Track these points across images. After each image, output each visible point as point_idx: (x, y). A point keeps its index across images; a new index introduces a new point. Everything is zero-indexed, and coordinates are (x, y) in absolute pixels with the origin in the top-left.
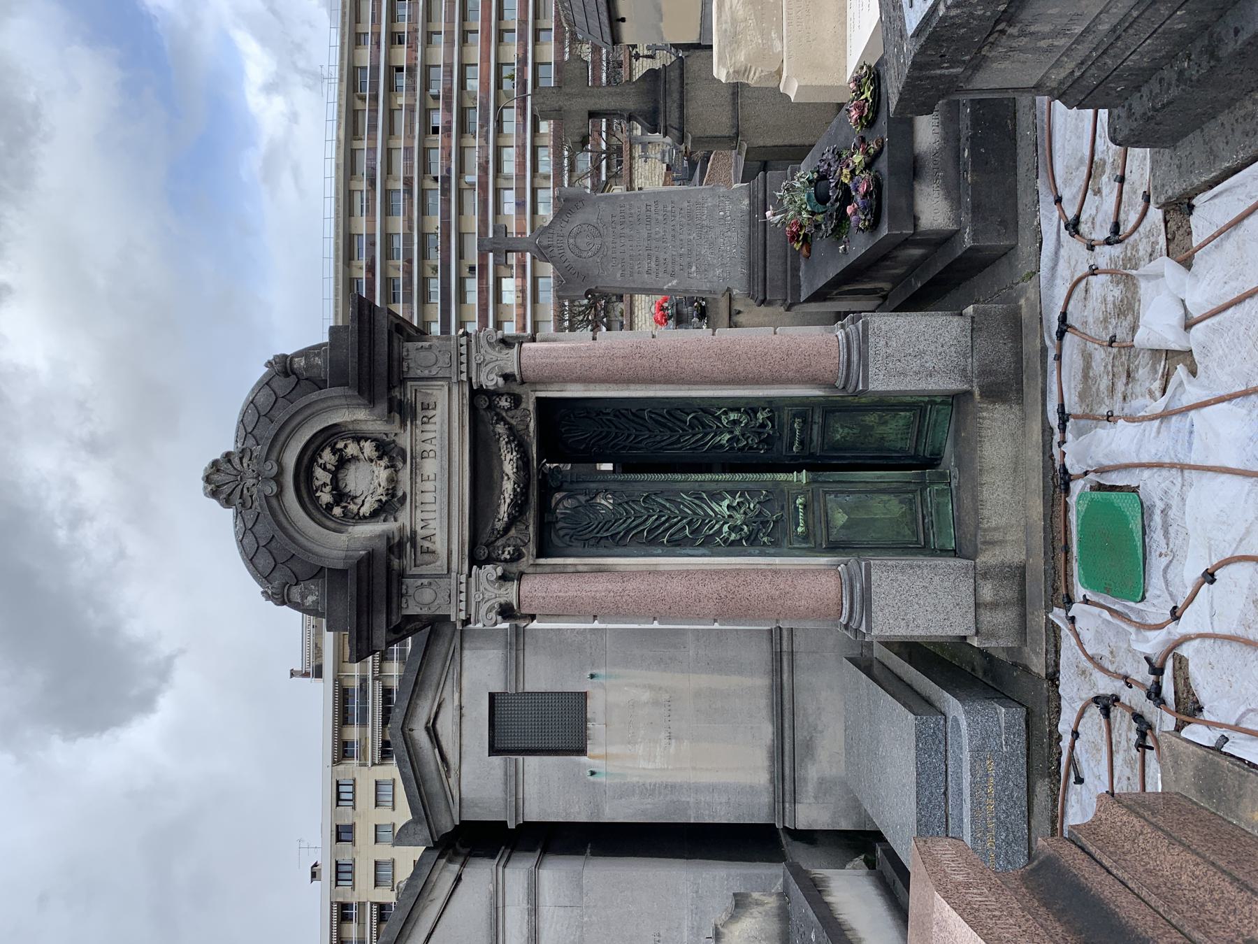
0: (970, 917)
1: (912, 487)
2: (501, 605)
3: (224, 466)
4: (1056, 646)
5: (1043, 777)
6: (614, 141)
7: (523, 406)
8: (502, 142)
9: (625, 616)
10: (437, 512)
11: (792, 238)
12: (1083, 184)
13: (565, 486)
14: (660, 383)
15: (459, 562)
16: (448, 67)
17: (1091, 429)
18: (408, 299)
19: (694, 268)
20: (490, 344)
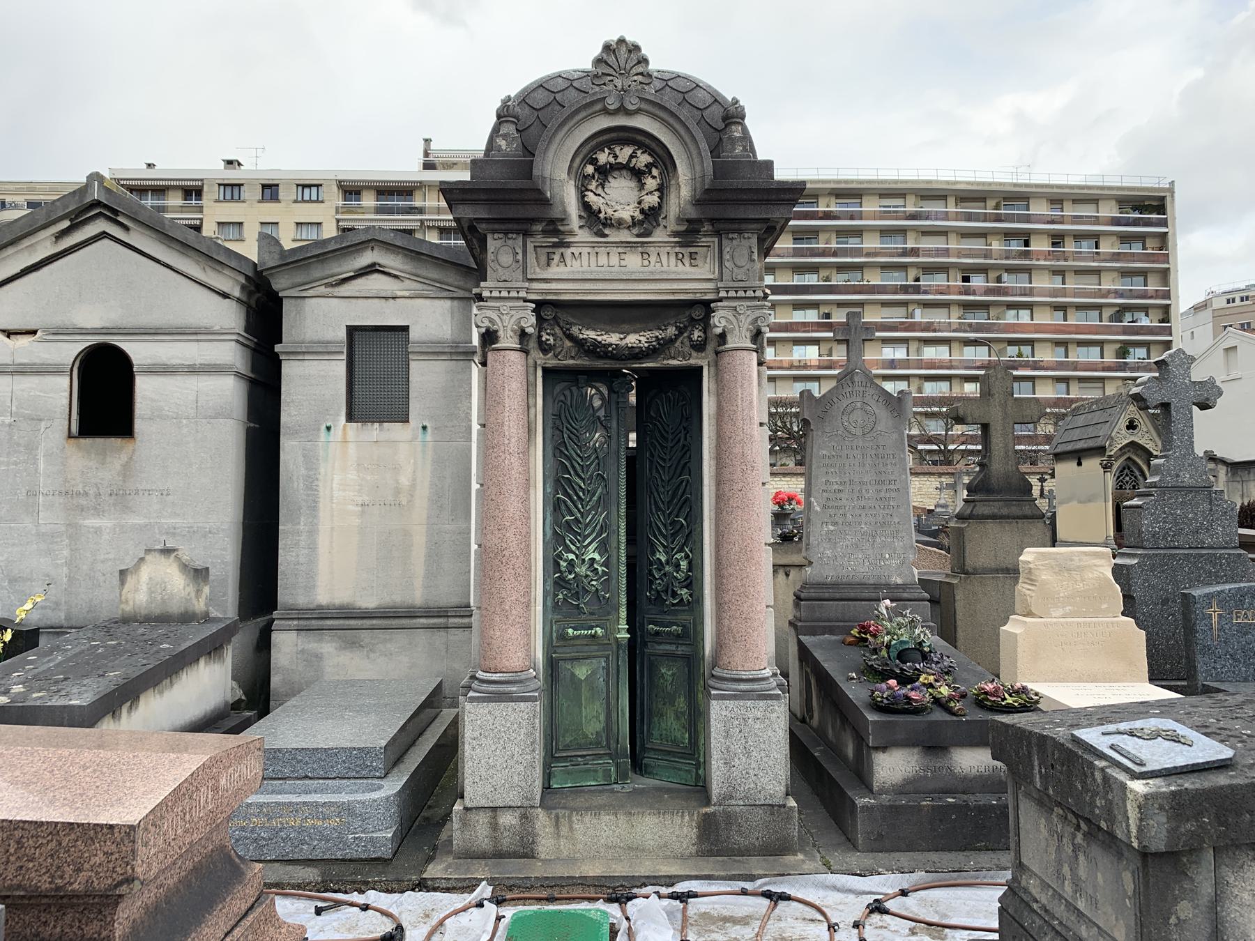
0: (184, 790)
1: (613, 745)
2: (496, 331)
3: (634, 57)
4: (454, 888)
5: (323, 874)
6: (957, 457)
7: (694, 354)
8: (955, 345)
9: (485, 456)
10: (590, 269)
11: (863, 627)
12: (921, 918)
13: (614, 396)
14: (717, 490)
15: (539, 290)
16: (1030, 292)
17: (672, 924)
18: (797, 253)
19: (832, 528)
20: (756, 320)
